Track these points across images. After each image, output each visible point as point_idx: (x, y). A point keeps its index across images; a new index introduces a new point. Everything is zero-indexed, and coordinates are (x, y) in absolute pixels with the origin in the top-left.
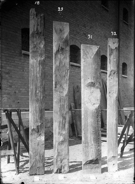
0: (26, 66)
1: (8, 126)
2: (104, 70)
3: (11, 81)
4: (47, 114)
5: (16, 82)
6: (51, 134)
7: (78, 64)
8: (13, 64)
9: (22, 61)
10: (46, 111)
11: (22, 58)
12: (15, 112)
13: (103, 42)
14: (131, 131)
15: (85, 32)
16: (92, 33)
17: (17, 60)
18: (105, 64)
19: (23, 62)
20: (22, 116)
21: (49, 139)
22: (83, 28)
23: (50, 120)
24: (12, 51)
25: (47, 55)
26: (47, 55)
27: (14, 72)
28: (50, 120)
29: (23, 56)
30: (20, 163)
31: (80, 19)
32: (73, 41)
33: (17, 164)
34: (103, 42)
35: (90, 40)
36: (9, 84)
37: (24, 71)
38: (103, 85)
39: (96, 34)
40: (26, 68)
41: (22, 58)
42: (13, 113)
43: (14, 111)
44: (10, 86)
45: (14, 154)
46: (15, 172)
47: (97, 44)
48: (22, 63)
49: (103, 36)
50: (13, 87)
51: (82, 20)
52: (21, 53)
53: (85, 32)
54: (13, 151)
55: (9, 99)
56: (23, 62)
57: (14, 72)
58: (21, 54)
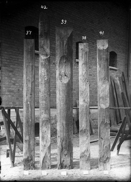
1: (4, 123)
2: (114, 67)
3: (14, 79)
5: (19, 80)
6: (55, 130)
8: (16, 62)
10: (36, 109)
12: (13, 109)
13: (113, 38)
14: (127, 128)
15: (92, 28)
18: (114, 61)
20: (35, 112)
21: (53, 135)
23: (54, 117)
24: (16, 50)
25: (52, 52)
26: (52, 52)
27: (18, 70)
28: (54, 117)
30: (35, 158)
31: (87, 15)
32: (79, 37)
33: (12, 158)
34: (113, 38)
35: (101, 35)
36: (12, 82)
38: (111, 82)
42: (11, 110)
43: (13, 108)
44: (14, 84)
45: (9, 149)
49: (113, 31)
50: (16, 84)
51: (89, 16)
53: (92, 28)
54: (9, 146)
55: (13, 96)
57: (18, 70)
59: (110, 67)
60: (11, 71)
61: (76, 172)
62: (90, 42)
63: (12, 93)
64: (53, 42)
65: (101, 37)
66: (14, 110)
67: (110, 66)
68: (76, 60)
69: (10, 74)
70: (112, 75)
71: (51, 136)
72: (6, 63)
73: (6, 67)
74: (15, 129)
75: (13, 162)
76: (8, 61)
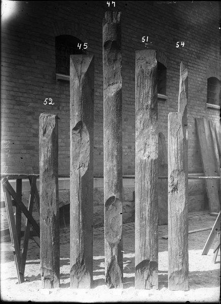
0: (62, 101)
4: (126, 183)
7: (163, 94)
9: (57, 92)
11: (57, 87)
16: (181, 40)
17: (47, 90)
19: (58, 94)
22: (173, 29)
29: (58, 83)
30: (26, 266)
37: (61, 109)
39: (199, 40)
40: (63, 105)
41: (57, 87)
42: (23, 180)
43: (26, 177)
46: (17, 281)
47: (200, 57)
48: (57, 96)
52: (55, 78)
56: (58, 94)
58: (55, 79)
59: (160, 95)
60: (30, 113)
61: (47, 290)
62: (190, 68)
63: (31, 151)
64: (129, 65)
65: (142, 47)
66: (28, 180)
67: (159, 93)
68: (206, 105)
69: (29, 118)
70: (211, 118)
71: (123, 223)
72: (22, 99)
73: (22, 106)
74: (29, 215)
75: (21, 273)
76: (25, 95)
